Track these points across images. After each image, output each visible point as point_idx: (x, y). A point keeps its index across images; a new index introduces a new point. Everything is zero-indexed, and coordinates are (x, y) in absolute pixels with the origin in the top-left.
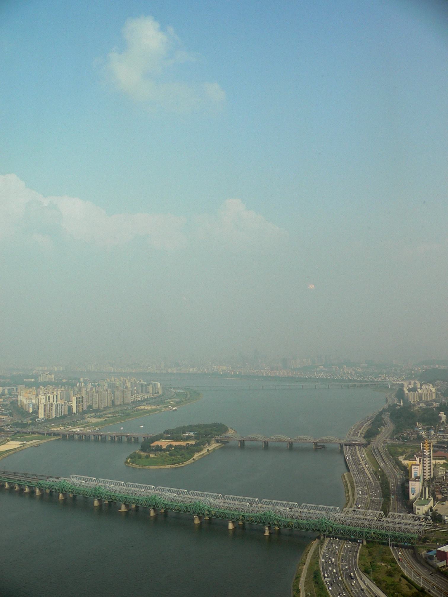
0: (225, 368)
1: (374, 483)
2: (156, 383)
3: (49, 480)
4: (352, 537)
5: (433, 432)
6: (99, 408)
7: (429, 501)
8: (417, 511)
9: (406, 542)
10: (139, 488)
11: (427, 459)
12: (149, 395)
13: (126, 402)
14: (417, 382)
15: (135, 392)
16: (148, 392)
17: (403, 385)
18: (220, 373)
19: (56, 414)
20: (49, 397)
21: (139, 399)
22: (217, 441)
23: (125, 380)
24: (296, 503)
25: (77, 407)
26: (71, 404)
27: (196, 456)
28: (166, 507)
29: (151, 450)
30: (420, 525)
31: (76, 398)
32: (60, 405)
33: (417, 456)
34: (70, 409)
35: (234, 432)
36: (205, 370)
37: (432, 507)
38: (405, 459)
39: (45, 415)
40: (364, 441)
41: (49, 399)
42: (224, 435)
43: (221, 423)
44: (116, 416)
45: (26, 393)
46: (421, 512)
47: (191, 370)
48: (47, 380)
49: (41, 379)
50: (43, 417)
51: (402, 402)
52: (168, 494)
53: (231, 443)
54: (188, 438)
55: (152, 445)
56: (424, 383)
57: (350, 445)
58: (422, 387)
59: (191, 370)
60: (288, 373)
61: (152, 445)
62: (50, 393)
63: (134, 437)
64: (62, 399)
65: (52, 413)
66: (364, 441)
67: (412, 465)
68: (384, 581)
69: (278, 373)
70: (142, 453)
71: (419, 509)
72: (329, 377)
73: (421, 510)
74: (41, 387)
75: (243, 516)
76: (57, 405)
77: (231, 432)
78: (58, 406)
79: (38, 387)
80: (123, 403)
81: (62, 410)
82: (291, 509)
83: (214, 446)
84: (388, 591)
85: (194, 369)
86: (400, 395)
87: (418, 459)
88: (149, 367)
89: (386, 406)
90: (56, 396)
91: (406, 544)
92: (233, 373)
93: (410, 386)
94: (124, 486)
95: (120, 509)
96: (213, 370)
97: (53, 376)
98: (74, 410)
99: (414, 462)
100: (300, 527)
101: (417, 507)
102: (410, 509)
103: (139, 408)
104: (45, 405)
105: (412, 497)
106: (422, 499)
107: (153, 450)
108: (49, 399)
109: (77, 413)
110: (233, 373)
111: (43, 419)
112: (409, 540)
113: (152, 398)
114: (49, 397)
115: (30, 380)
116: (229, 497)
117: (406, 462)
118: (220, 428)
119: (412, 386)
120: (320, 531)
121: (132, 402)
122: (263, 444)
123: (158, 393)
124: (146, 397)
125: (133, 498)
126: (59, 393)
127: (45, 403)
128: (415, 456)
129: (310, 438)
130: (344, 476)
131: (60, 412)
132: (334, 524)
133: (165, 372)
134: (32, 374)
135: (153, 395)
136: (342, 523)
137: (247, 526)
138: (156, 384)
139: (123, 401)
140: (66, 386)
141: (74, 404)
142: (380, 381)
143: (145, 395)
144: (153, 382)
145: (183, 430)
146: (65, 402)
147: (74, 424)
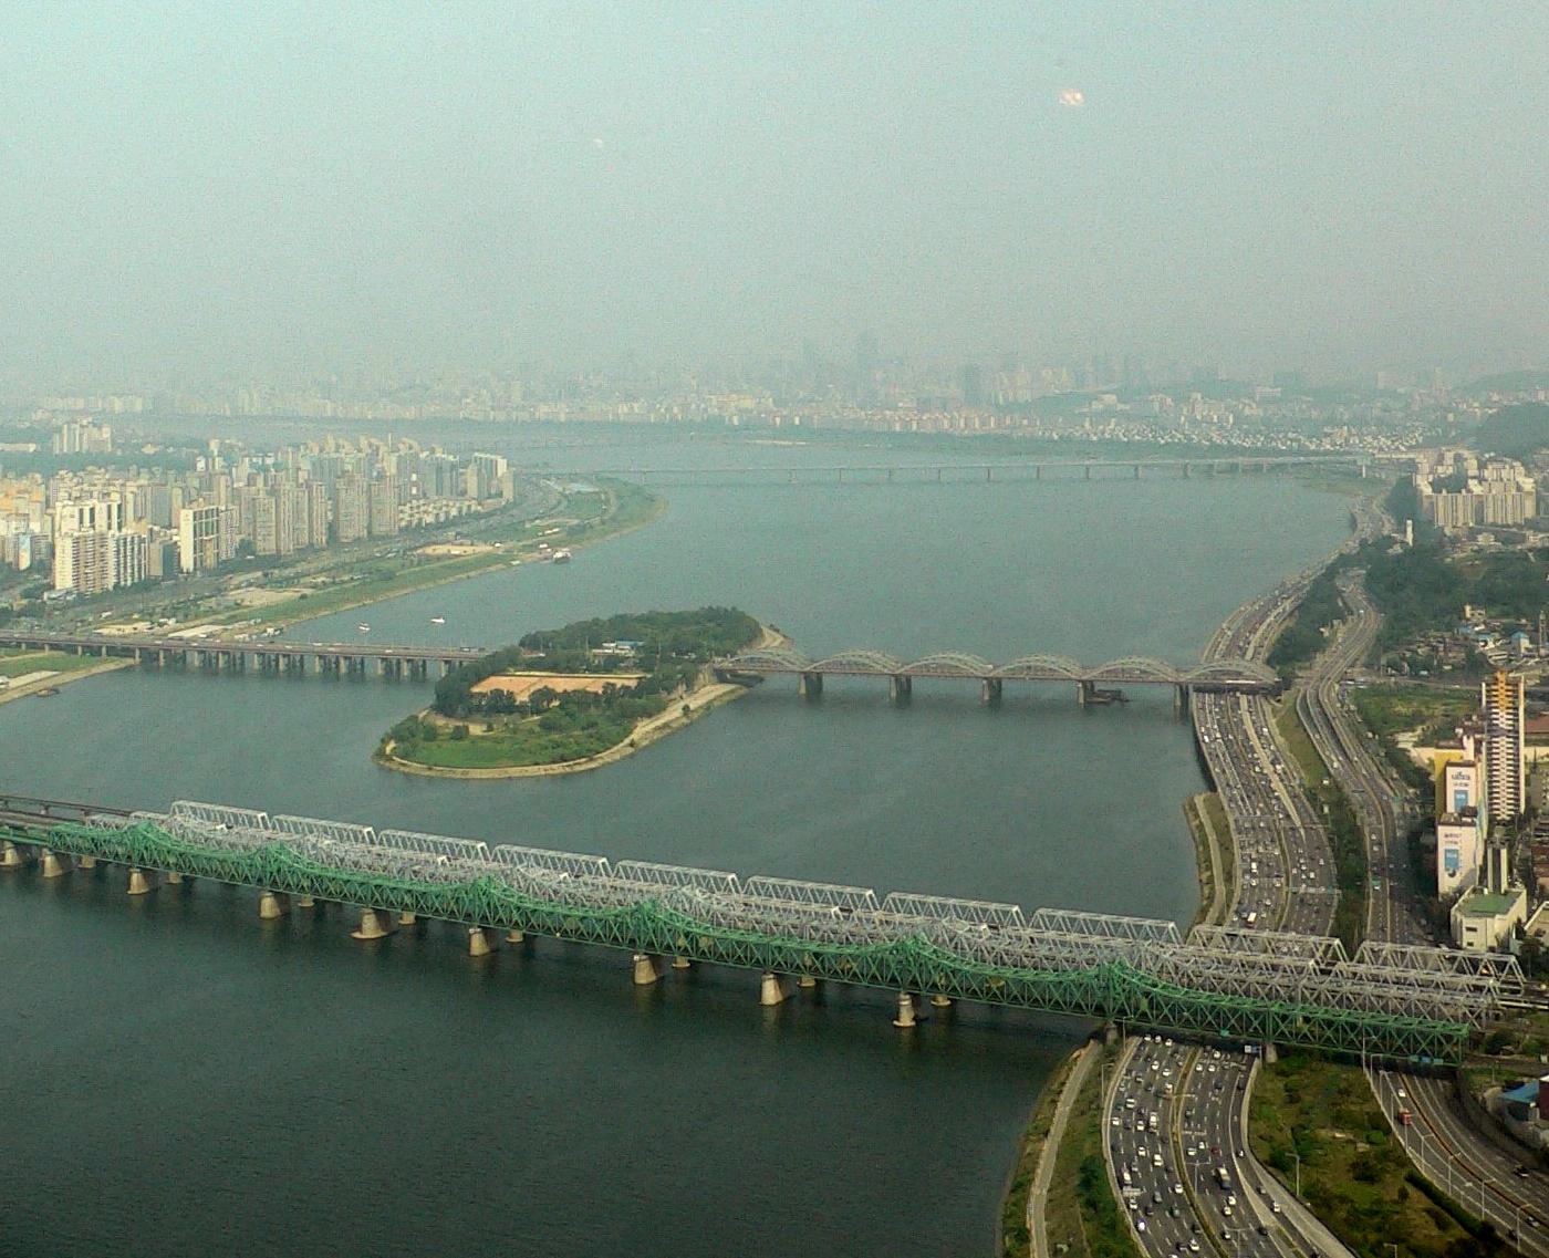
0: (748, 403)
1: (1306, 832)
2: (493, 457)
3: (93, 822)
4: (1225, 1033)
5: (1525, 643)
6: (278, 551)
7: (1510, 898)
8: (1467, 937)
9: (1424, 1053)
10: (428, 850)
11: (1503, 743)
12: (467, 503)
13: (377, 530)
14: (1466, 454)
15: (414, 491)
16: (464, 493)
17: (1412, 466)
18: (730, 420)
19: (118, 575)
20: (92, 510)
21: (430, 519)
22: (721, 676)
23: (378, 448)
24: (1016, 908)
25: (199, 547)
26: (175, 538)
27: (643, 730)
28: (529, 920)
29: (474, 709)
30: (1478, 989)
31: (195, 513)
32: (133, 541)
33: (1465, 733)
34: (171, 554)
35: (782, 642)
36: (676, 410)
37: (1524, 920)
38: (1422, 743)
39: (76, 579)
40: (1270, 677)
41: (92, 519)
42: (745, 654)
43: (734, 609)
44: (343, 582)
45: (7, 496)
46: (1483, 940)
47: (623, 409)
48: (85, 447)
49: (62, 445)
50: (69, 584)
51: (1409, 529)
52: (536, 873)
53: (774, 683)
54: (612, 664)
55: (476, 690)
56: (1491, 460)
57: (1218, 691)
58: (1486, 473)
59: (623, 409)
60: (983, 424)
61: (476, 690)
62: (95, 494)
63: (408, 661)
64: (140, 519)
65: (103, 571)
66: (1270, 677)
67: (1449, 764)
68: (1343, 1199)
69: (946, 422)
70: (440, 721)
71: (1474, 930)
72: (1137, 437)
73: (1483, 932)
74: (62, 472)
75: (817, 955)
76: (122, 543)
77: (771, 643)
78: (125, 543)
79: (49, 476)
80: (369, 533)
81: (140, 561)
82: (996, 928)
83: (709, 692)
84: (1358, 1235)
85: (635, 405)
86: (1404, 502)
87: (1469, 743)
88: (467, 397)
89: (1352, 546)
90: (119, 507)
91: (1426, 1060)
92: (778, 420)
93: (1440, 469)
94: (372, 842)
95: (359, 928)
96: (705, 410)
97: (106, 433)
98: (187, 561)
99: (1454, 755)
100: (1026, 995)
101: (1467, 923)
102: (1442, 929)
103: (429, 550)
104: (77, 541)
105: (1446, 884)
106: (1486, 891)
107: (479, 709)
108: (92, 519)
109: (195, 569)
110: (778, 420)
111: (69, 593)
112: (1437, 1044)
113: (478, 516)
114: (92, 510)
115: (21, 447)
116: (763, 885)
117: (1423, 755)
118: (731, 628)
119: (1446, 470)
120: (1104, 1012)
121: (401, 530)
122: (893, 685)
123: (500, 495)
124: (454, 512)
125: (407, 887)
126: (130, 497)
127: (76, 534)
128: (1460, 731)
129: (1067, 666)
130: (1193, 807)
131: (133, 566)
132: (1155, 986)
133: (525, 416)
134: (28, 424)
135: (480, 504)
136: (1185, 980)
137: (831, 993)
138: (494, 464)
139: (369, 528)
140: (154, 469)
141: (185, 539)
142: (1327, 453)
143: (451, 504)
144: (482, 455)
145: (593, 633)
146: (151, 530)
147: (186, 612)
